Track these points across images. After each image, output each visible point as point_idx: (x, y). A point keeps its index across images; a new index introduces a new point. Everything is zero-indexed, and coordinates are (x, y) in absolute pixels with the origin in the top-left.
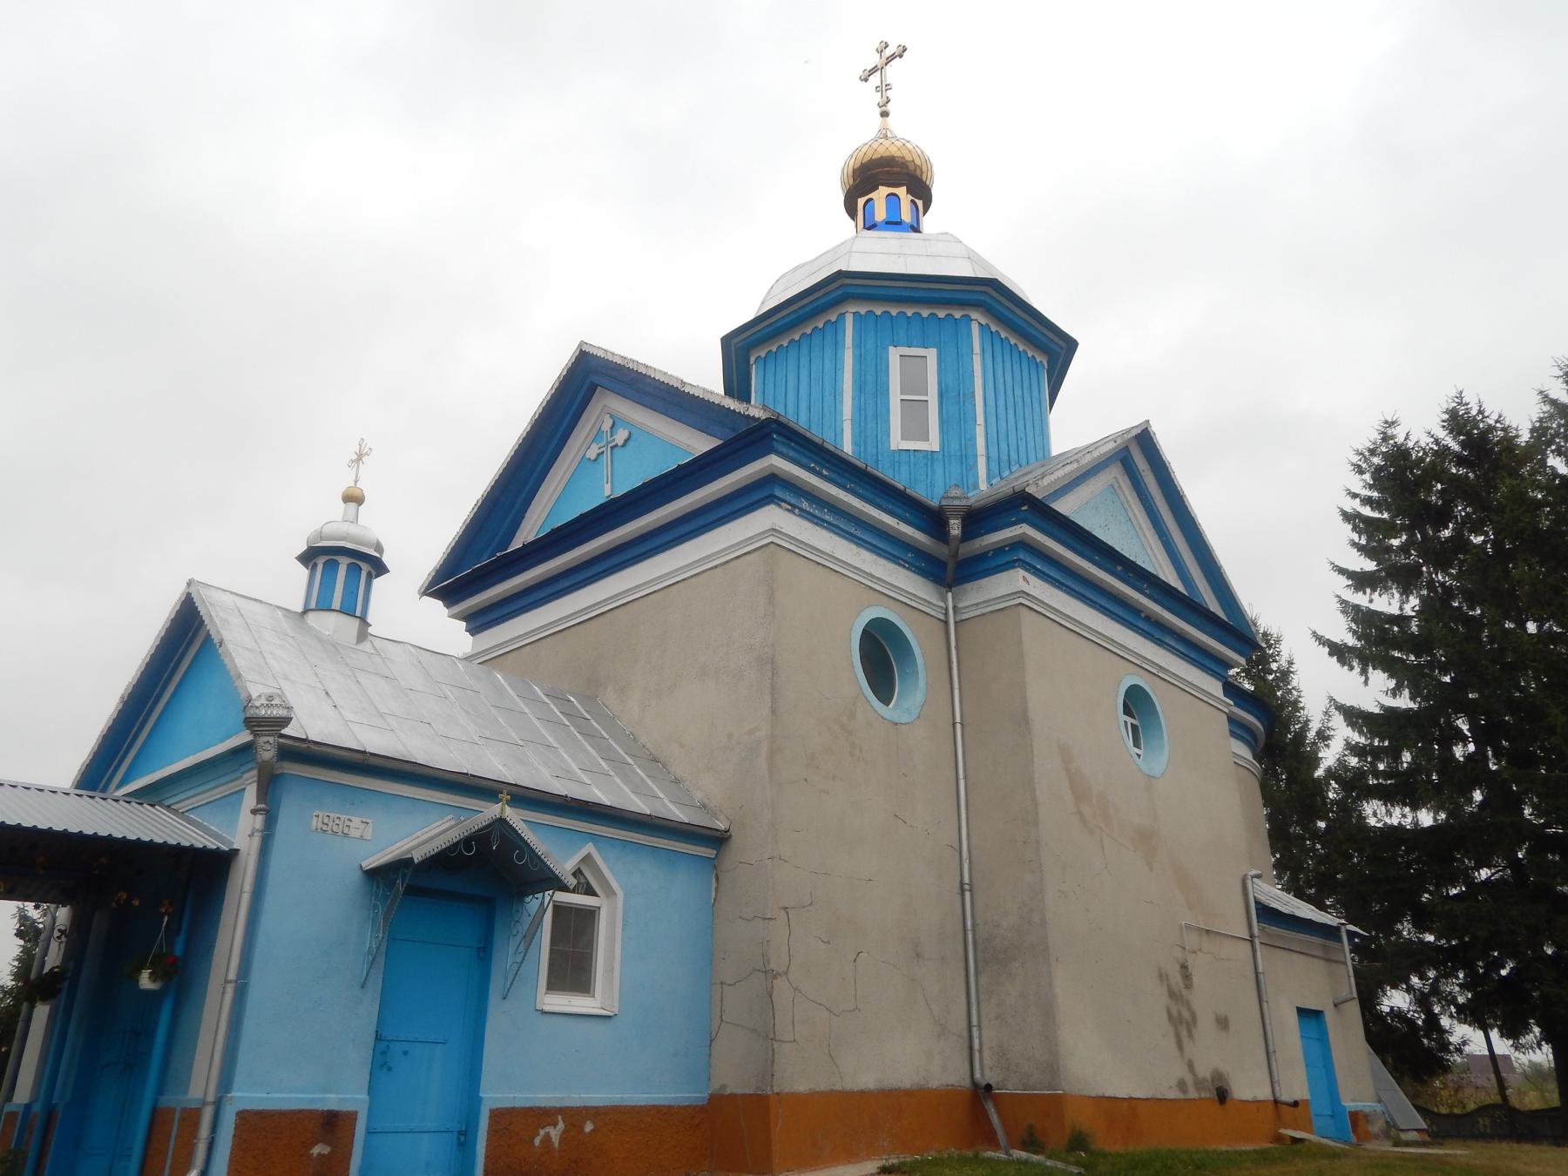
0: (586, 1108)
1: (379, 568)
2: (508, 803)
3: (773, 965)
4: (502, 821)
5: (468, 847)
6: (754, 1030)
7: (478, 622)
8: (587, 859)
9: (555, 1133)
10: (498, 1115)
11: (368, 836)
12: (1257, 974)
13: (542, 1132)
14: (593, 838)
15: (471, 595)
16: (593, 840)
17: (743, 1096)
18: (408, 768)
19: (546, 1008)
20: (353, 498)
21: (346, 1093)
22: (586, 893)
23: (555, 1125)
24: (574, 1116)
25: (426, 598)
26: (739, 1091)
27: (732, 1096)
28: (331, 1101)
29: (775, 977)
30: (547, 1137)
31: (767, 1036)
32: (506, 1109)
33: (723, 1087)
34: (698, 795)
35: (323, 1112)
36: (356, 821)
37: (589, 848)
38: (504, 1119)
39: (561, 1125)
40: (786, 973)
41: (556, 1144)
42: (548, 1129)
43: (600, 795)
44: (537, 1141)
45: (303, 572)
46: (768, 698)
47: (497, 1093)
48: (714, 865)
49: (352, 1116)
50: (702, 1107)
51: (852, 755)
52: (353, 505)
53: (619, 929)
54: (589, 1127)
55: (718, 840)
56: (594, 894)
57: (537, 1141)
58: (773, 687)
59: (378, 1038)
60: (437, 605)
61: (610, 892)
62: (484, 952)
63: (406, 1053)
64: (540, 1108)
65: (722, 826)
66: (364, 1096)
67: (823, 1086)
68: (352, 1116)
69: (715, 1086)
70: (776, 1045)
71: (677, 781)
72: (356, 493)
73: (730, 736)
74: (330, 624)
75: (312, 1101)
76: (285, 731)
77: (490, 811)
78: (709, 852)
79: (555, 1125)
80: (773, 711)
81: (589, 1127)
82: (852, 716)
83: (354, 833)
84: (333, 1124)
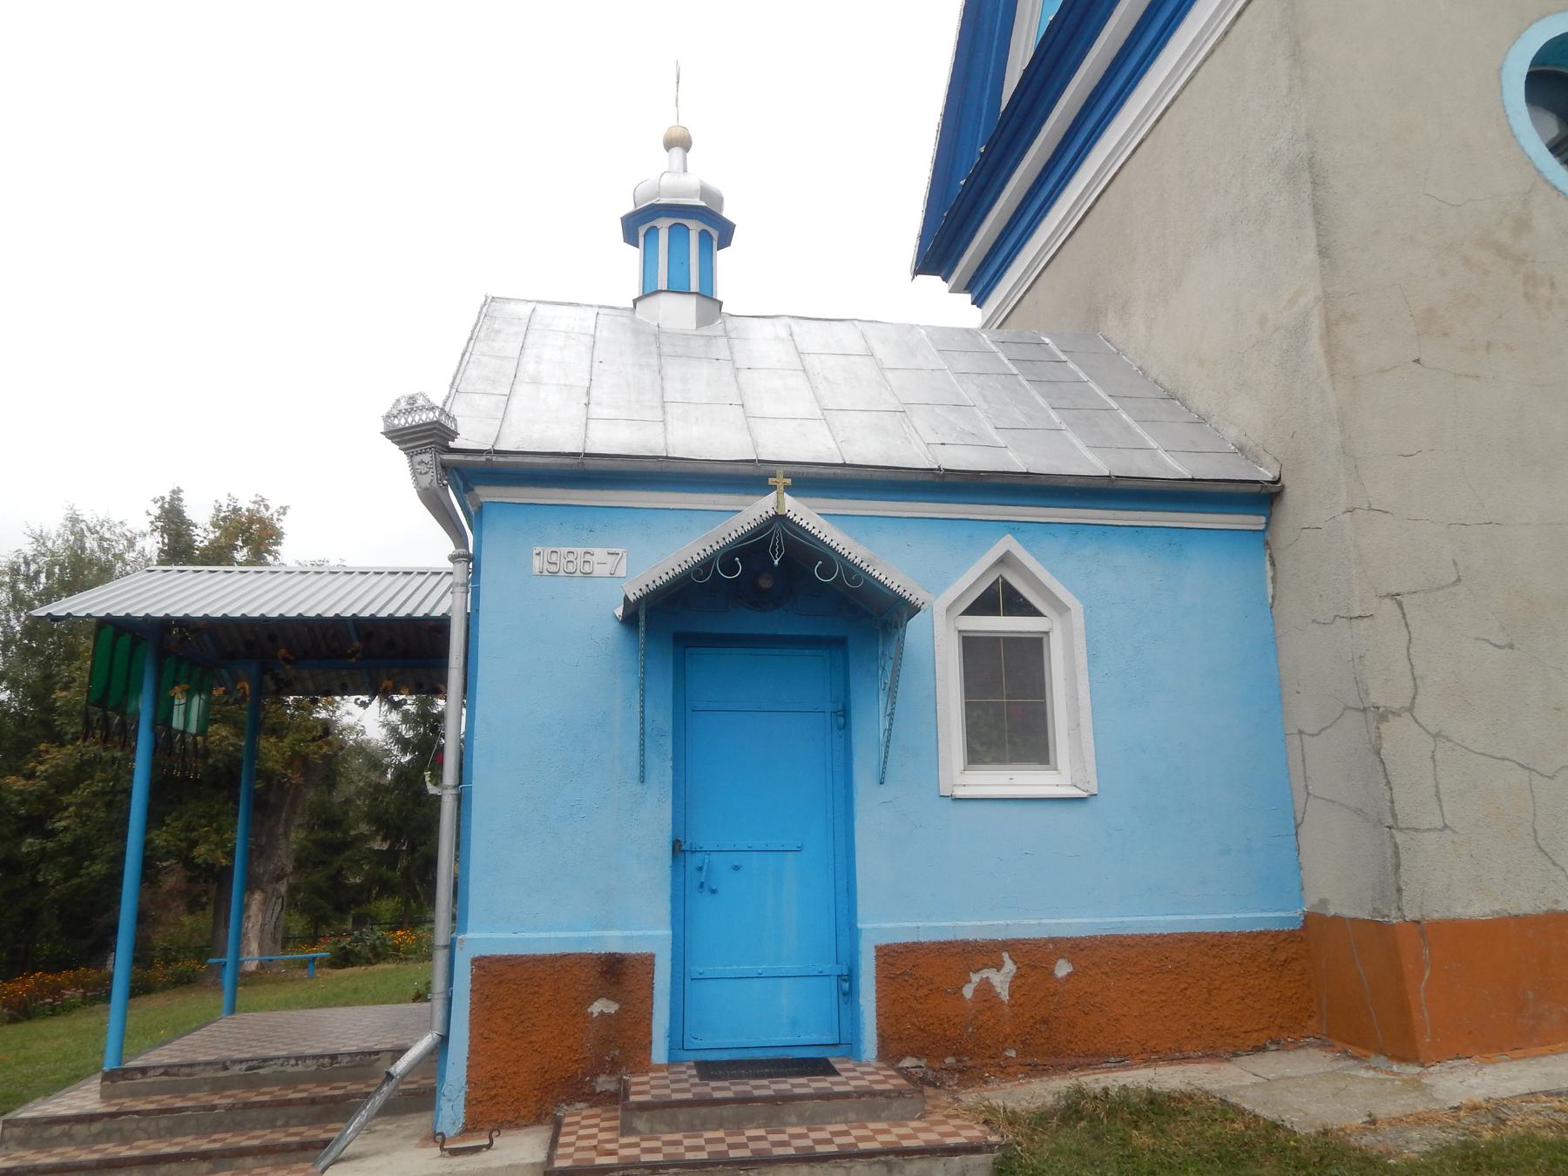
0: (1054, 941)
1: (725, 231)
2: (787, 489)
3: (1375, 698)
4: (780, 519)
5: (729, 567)
6: (1358, 811)
7: (979, 287)
8: (1005, 560)
9: (1001, 979)
10: (889, 956)
11: (622, 571)
12: (1503, 759)
13: (975, 978)
14: (1012, 526)
15: (961, 254)
16: (1013, 531)
17: (1354, 920)
18: (651, 466)
19: (959, 793)
20: (679, 142)
21: (640, 927)
22: (1010, 612)
23: (999, 966)
24: (1033, 956)
25: (920, 277)
26: (1347, 913)
27: (1337, 919)
28: (613, 941)
29: (1383, 718)
30: (986, 986)
31: (1387, 823)
32: (906, 945)
33: (1323, 902)
34: (1232, 433)
35: (599, 957)
36: (600, 553)
37: (1007, 543)
38: (900, 963)
39: (1010, 967)
40: (1411, 709)
41: (1005, 996)
42: (985, 973)
43: (1017, 460)
44: (968, 991)
45: (634, 255)
46: (1310, 232)
47: (886, 920)
48: (1264, 539)
49: (647, 961)
50: (1292, 933)
51: (1529, 297)
52: (677, 152)
53: (1082, 662)
54: (1063, 969)
55: (1263, 498)
56: (1033, 612)
57: (968, 991)
58: (1317, 209)
59: (677, 848)
60: (934, 282)
61: (1061, 608)
62: (843, 717)
63: (736, 868)
64: (966, 943)
65: (1267, 474)
66: (666, 932)
67: (1526, 903)
68: (647, 961)
69: (1310, 903)
70: (1400, 837)
71: (1202, 420)
72: (677, 133)
73: (1263, 321)
74: (678, 311)
75: (581, 940)
76: (451, 444)
77: (755, 510)
78: (1255, 521)
79: (999, 966)
80: (1323, 252)
81: (1063, 969)
82: (1522, 225)
83: (599, 571)
84: (617, 972)
